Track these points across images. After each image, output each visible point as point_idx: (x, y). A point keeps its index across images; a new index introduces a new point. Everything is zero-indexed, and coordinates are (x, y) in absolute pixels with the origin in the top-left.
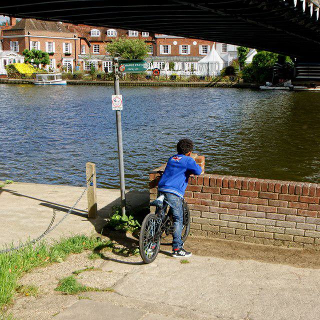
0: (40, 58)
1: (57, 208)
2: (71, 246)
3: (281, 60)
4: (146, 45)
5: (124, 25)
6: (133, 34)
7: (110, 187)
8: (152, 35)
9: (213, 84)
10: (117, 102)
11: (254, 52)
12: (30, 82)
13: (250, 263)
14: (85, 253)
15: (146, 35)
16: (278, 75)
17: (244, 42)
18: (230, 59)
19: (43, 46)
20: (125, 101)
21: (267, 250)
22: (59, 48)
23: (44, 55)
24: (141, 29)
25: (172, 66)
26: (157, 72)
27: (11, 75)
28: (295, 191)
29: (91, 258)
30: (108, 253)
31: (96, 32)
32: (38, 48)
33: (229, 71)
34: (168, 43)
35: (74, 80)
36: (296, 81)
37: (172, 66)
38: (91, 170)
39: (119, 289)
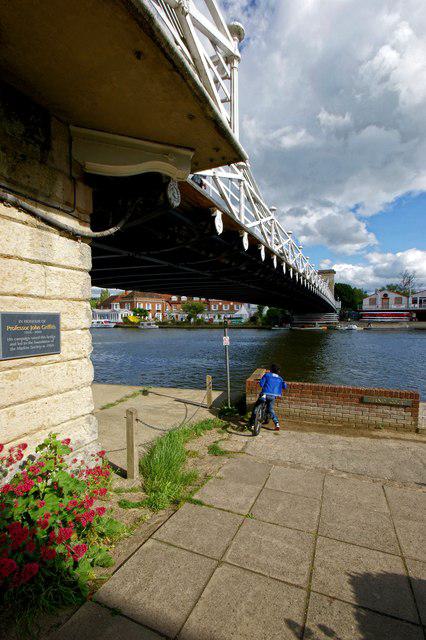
0: (143, 313)
1: (186, 402)
2: (205, 425)
3: (283, 312)
4: (204, 306)
5: (190, 295)
6: (196, 299)
7: (384, 400)
8: (207, 299)
9: (244, 327)
10: (226, 341)
11: (267, 308)
12: (135, 326)
13: (314, 434)
14: (214, 430)
15: (203, 299)
16: (286, 320)
17: (261, 303)
18: (253, 312)
19: (144, 306)
20: (222, 340)
21: (320, 426)
22: (153, 307)
23: (145, 311)
24: (200, 296)
25: (219, 317)
26: (211, 320)
27: (125, 323)
28: (317, 389)
29: (219, 432)
30: (229, 429)
31: (174, 298)
32: (142, 307)
33: (253, 319)
34: (216, 305)
35: (163, 325)
36: (293, 324)
37: (219, 317)
38: (209, 379)
39: (247, 451)
